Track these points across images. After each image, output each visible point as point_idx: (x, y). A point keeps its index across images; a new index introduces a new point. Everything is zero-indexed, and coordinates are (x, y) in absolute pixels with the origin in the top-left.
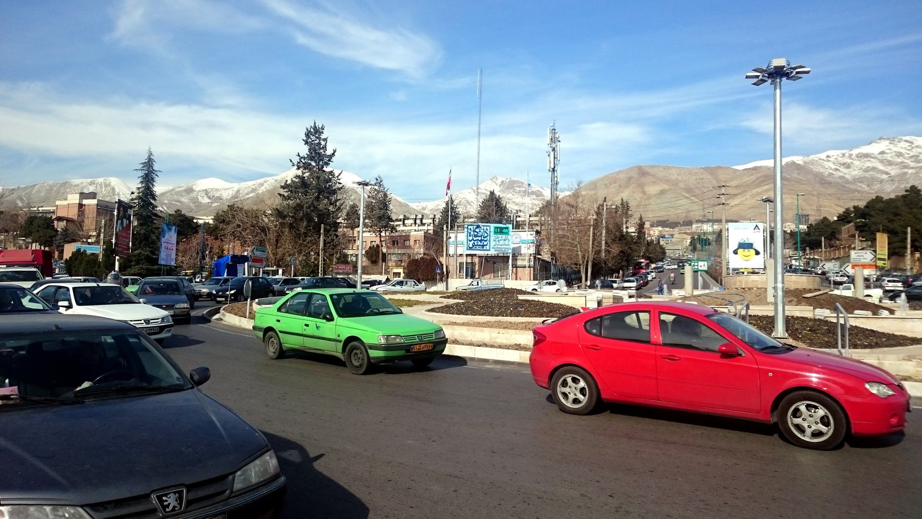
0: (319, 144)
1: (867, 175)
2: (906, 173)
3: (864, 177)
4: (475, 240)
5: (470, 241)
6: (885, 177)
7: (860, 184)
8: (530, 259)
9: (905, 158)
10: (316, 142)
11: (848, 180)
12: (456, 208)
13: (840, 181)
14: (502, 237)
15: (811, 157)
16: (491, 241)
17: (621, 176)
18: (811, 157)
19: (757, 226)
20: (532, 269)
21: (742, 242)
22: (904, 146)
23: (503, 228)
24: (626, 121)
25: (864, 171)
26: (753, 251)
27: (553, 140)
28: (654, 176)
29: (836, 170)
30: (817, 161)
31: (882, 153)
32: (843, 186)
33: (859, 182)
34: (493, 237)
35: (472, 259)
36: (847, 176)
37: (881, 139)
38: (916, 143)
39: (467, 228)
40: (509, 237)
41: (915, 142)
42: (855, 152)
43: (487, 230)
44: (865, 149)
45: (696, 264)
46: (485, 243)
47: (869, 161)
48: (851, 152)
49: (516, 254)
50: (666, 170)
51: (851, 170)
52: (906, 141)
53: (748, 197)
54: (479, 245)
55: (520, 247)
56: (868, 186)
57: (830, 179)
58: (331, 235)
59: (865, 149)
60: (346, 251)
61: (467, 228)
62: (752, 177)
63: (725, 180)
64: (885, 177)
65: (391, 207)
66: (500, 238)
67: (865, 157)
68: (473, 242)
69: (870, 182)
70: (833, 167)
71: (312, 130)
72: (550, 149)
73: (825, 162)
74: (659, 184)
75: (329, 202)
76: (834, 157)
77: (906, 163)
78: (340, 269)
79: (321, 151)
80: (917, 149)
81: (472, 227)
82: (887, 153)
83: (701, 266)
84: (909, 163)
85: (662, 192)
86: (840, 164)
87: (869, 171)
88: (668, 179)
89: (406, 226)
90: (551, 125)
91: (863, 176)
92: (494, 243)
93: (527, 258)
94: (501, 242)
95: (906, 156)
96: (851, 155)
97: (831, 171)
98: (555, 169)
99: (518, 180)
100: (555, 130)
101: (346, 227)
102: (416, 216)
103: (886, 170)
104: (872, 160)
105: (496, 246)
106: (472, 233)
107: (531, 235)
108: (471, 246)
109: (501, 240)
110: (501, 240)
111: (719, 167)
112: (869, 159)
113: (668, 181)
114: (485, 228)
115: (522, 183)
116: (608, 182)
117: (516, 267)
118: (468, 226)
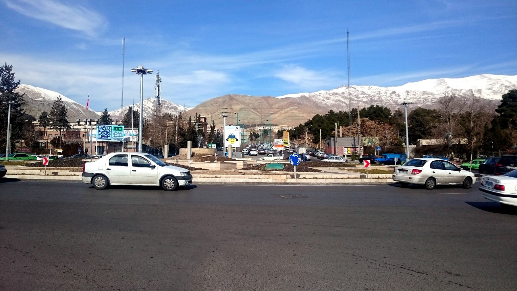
0: (9, 76)
1: (337, 103)
2: (353, 103)
3: (335, 104)
4: (103, 134)
5: (100, 134)
6: (344, 104)
7: (333, 108)
8: (134, 144)
9: (352, 96)
10: (7, 75)
11: (328, 106)
12: (109, 116)
13: (325, 106)
14: (118, 132)
15: (312, 93)
16: (112, 134)
17: (220, 100)
18: (312, 94)
19: (237, 127)
20: (135, 149)
21: (230, 135)
22: (352, 90)
23: (119, 128)
24: (217, 70)
25: (335, 101)
26: (235, 139)
27: (158, 81)
28: (237, 100)
29: (323, 100)
30: (315, 96)
31: (343, 93)
32: (326, 109)
33: (333, 107)
34: (113, 132)
35: (102, 144)
36: (328, 104)
37: (342, 86)
38: (357, 89)
39: (98, 127)
40: (122, 132)
41: (357, 88)
42: (331, 92)
43: (110, 128)
44: (336, 91)
45: (211, 146)
46: (109, 136)
47: (337, 96)
48: (330, 92)
49: (127, 141)
50: (243, 98)
51: (330, 100)
52: (353, 88)
53: (283, 113)
54: (105, 137)
55: (130, 137)
56: (337, 109)
57: (320, 105)
58: (17, 130)
59: (336, 91)
60: (38, 140)
61: (98, 127)
62: (285, 103)
63: (272, 103)
64: (344, 104)
65: (67, 114)
66: (117, 133)
67: (335, 94)
68: (101, 135)
69: (339, 106)
70: (322, 99)
71: (4, 68)
72: (156, 86)
73: (318, 97)
74: (240, 105)
75: (16, 111)
76: (323, 94)
77: (353, 98)
78: (23, 150)
79: (10, 81)
80: (358, 92)
81: (101, 127)
82: (345, 93)
83: (213, 147)
84: (354, 98)
85: (241, 109)
86: (325, 97)
87: (337, 101)
88: (244, 102)
89: (80, 126)
90: (157, 73)
91: (335, 104)
92: (114, 136)
93: (132, 143)
94: (118, 135)
95: (353, 95)
96: (330, 93)
97: (321, 101)
98: (159, 96)
99: (163, 100)
100: (159, 75)
101: (40, 126)
102: (87, 120)
103: (345, 101)
104: (339, 96)
105: (115, 137)
106: (101, 130)
107: (135, 131)
108: (100, 137)
109: (117, 134)
110: (117, 134)
111: (269, 97)
112: (337, 95)
113: (244, 103)
114: (109, 127)
115: (166, 102)
116: (213, 103)
117: (127, 148)
118: (99, 126)
